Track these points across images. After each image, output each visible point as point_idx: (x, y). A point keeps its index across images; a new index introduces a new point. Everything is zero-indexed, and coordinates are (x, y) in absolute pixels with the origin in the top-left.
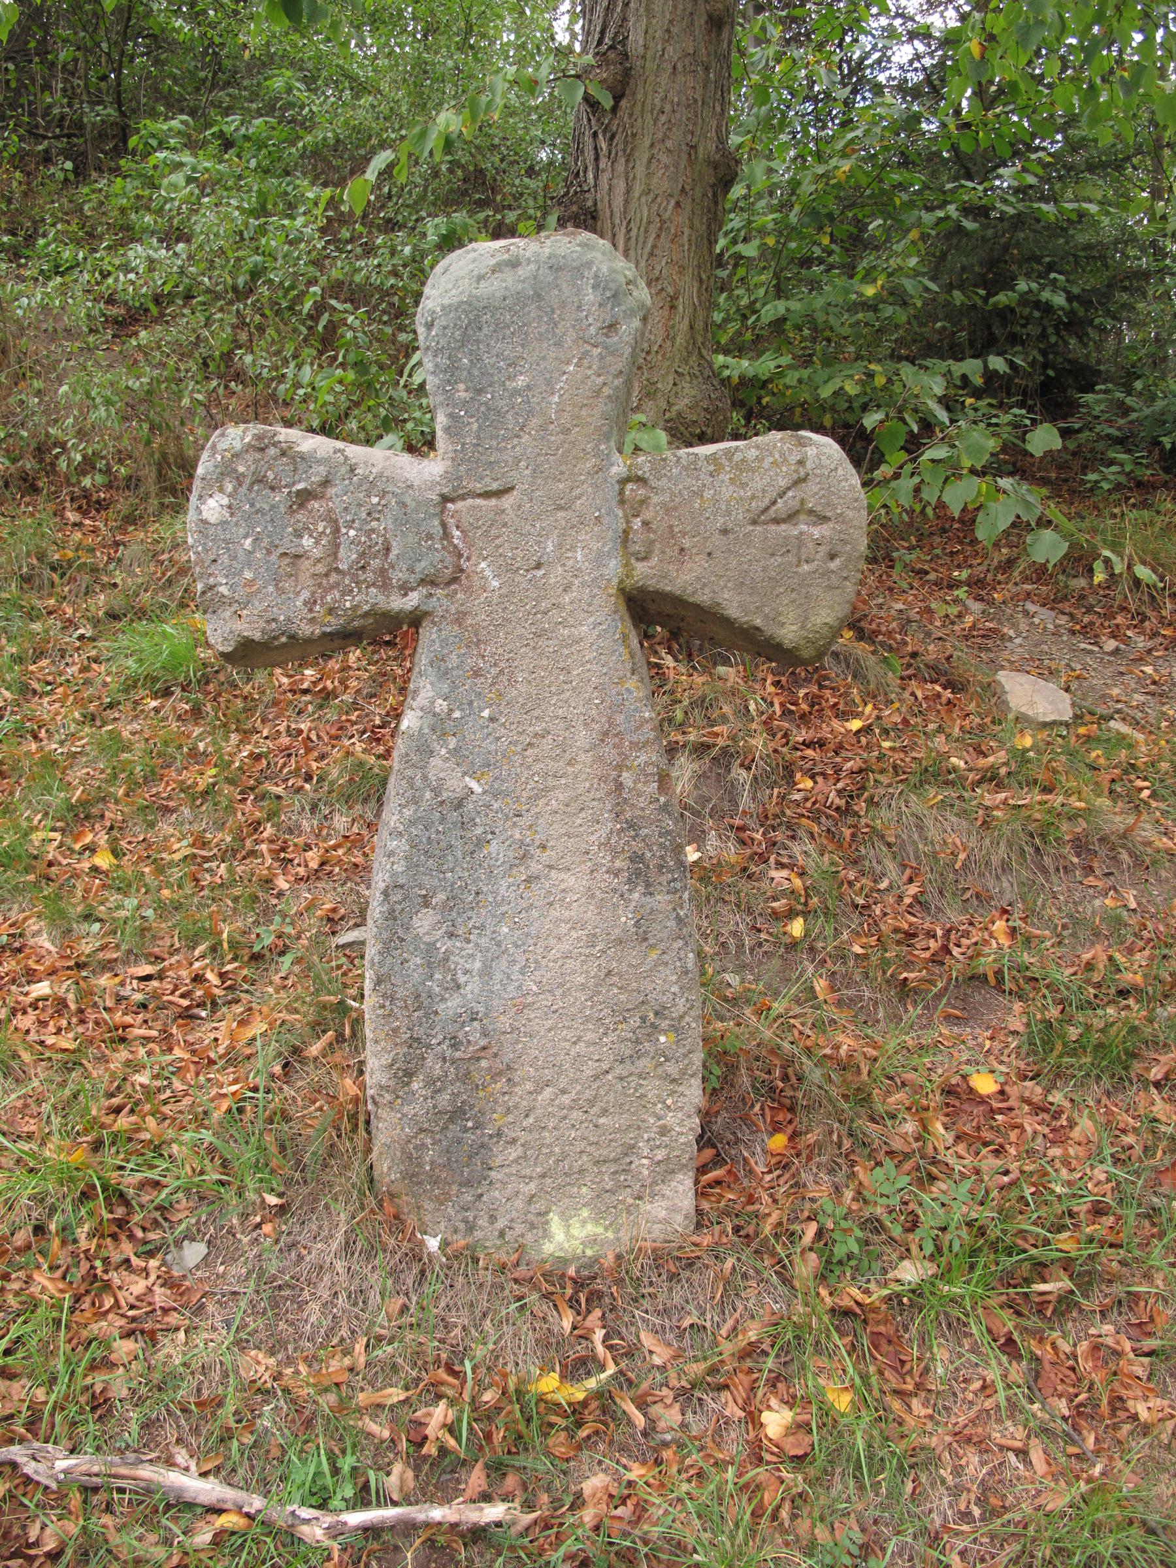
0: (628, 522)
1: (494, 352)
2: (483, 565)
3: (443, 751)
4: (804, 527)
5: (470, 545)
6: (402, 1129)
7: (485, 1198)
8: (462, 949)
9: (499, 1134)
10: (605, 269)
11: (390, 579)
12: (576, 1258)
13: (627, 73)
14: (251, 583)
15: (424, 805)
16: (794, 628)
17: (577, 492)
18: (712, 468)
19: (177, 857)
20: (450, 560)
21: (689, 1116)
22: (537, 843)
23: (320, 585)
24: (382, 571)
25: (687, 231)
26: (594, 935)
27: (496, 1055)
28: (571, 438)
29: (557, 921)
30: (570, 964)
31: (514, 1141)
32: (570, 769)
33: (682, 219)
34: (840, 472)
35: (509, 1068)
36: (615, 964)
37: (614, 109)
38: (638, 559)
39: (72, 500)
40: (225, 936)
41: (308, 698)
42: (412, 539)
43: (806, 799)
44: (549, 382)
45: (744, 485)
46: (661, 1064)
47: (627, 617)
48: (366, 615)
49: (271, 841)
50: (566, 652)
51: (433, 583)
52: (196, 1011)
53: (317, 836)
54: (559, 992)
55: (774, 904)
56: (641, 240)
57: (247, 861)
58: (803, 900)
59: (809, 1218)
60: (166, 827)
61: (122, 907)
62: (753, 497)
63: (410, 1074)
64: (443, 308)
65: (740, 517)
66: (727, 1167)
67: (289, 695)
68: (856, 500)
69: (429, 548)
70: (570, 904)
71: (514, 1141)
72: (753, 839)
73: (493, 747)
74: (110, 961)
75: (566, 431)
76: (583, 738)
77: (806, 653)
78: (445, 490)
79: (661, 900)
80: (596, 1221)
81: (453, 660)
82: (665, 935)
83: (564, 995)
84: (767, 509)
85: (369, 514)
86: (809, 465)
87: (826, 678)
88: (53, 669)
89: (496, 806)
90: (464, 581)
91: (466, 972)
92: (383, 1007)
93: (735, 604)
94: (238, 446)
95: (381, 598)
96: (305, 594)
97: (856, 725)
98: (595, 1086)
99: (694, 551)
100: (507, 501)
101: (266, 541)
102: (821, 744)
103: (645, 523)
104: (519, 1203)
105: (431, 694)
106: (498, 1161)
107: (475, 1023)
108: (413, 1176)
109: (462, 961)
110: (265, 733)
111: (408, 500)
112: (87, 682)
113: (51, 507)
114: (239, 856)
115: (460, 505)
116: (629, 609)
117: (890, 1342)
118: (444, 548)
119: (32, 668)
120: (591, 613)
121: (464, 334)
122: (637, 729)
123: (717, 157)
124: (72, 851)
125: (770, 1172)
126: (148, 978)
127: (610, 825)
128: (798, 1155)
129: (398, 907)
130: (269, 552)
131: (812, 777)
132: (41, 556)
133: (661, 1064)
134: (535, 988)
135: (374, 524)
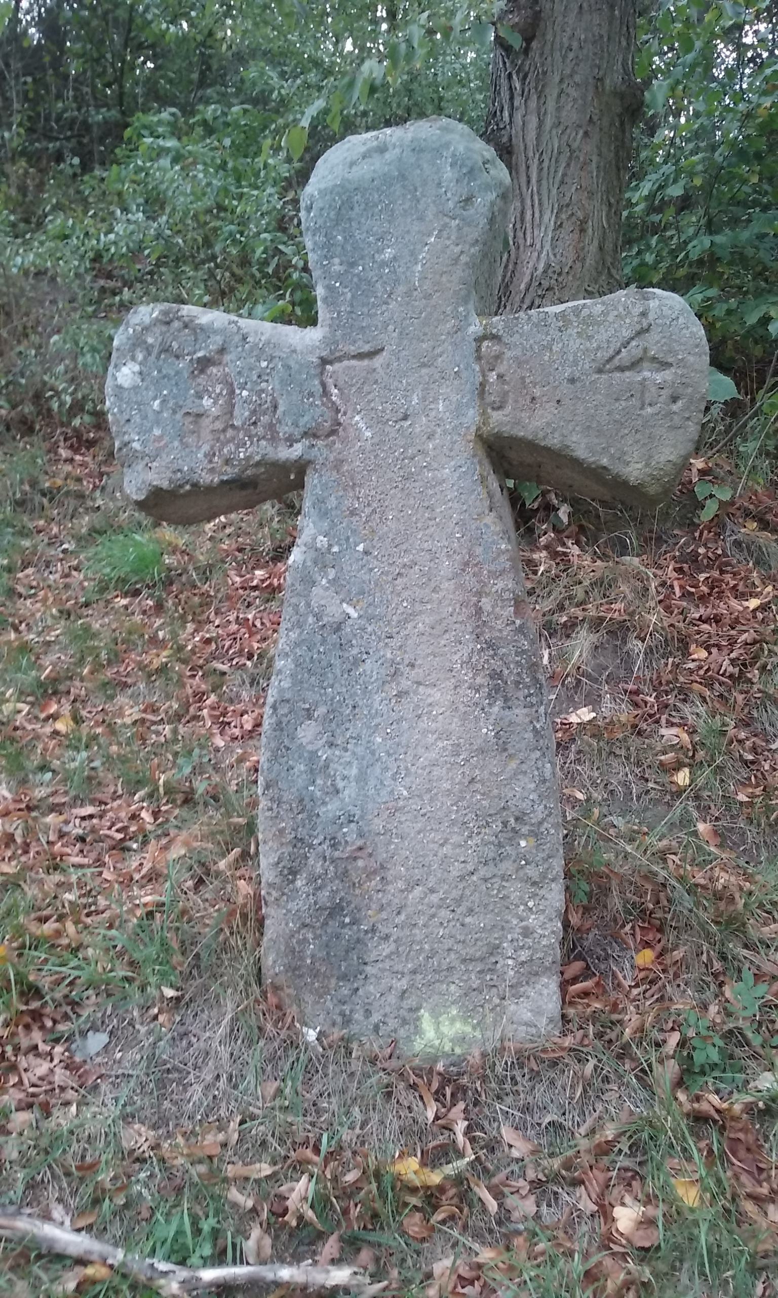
0: (484, 376)
1: (365, 228)
2: (357, 418)
3: (324, 581)
4: (647, 374)
5: (347, 401)
6: (287, 924)
7: (360, 992)
8: (340, 757)
9: (373, 930)
10: (461, 148)
11: (278, 433)
12: (446, 1055)
13: (537, 17)
14: (160, 438)
15: (307, 629)
16: (639, 466)
17: (438, 350)
18: (561, 324)
19: (128, 721)
20: (329, 414)
21: (551, 920)
22: (406, 662)
23: (218, 440)
24: (271, 426)
25: (595, 158)
26: (458, 745)
27: (370, 855)
28: (433, 302)
29: (425, 732)
30: (436, 772)
31: (387, 937)
32: (435, 596)
33: (589, 147)
34: (681, 320)
35: (382, 867)
36: (477, 772)
37: (526, 51)
38: (493, 409)
39: (65, 440)
40: (161, 782)
41: (257, 593)
42: (296, 397)
43: (700, 668)
44: (413, 253)
45: (589, 338)
46: (522, 867)
47: (486, 462)
48: (258, 464)
49: (213, 708)
50: (431, 492)
51: (315, 436)
52: (128, 844)
53: (254, 705)
54: (426, 797)
55: (663, 758)
56: (552, 170)
57: (190, 725)
58: (690, 754)
59: (673, 1029)
60: (122, 699)
61: (74, 760)
62: (599, 348)
63: (294, 872)
64: (320, 192)
65: (587, 366)
66: (596, 979)
67: (241, 591)
68: (697, 346)
69: (311, 404)
70: (436, 716)
71: (387, 937)
72: (646, 703)
73: (367, 577)
74: (58, 805)
75: (428, 297)
76: (446, 566)
77: (653, 489)
78: (324, 354)
79: (519, 714)
80: (465, 1019)
81: (332, 502)
82: (523, 745)
83: (431, 800)
84: (611, 358)
85: (259, 377)
86: (651, 316)
87: (728, 564)
88: (38, 576)
89: (370, 629)
90: (341, 433)
91: (344, 778)
92: (271, 809)
93: (583, 446)
94: (147, 320)
95: (270, 449)
96: (206, 448)
97: (753, 603)
98: (461, 886)
99: (544, 399)
100: (378, 361)
101: (171, 404)
102: (717, 619)
103: (500, 376)
104: (392, 999)
105: (313, 531)
106: (373, 956)
107: (352, 825)
108: (295, 969)
109: (340, 768)
110: (217, 624)
111: (292, 363)
112: (67, 586)
113: (46, 445)
114: (183, 721)
115: (337, 366)
116: (489, 456)
117: (748, 1150)
118: (323, 404)
119: (20, 575)
120: (452, 458)
121: (338, 214)
122: (494, 559)
123: (623, 88)
124: (36, 718)
125: (637, 986)
126: (91, 817)
127: (471, 646)
128: (664, 971)
129: (285, 720)
130: (174, 412)
131: (708, 649)
132: (34, 484)
133: (522, 867)
134: (405, 793)
135: (264, 385)
